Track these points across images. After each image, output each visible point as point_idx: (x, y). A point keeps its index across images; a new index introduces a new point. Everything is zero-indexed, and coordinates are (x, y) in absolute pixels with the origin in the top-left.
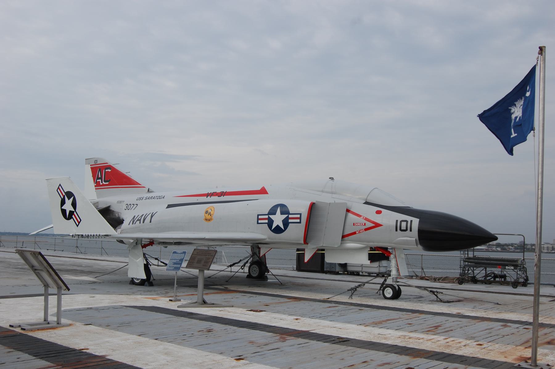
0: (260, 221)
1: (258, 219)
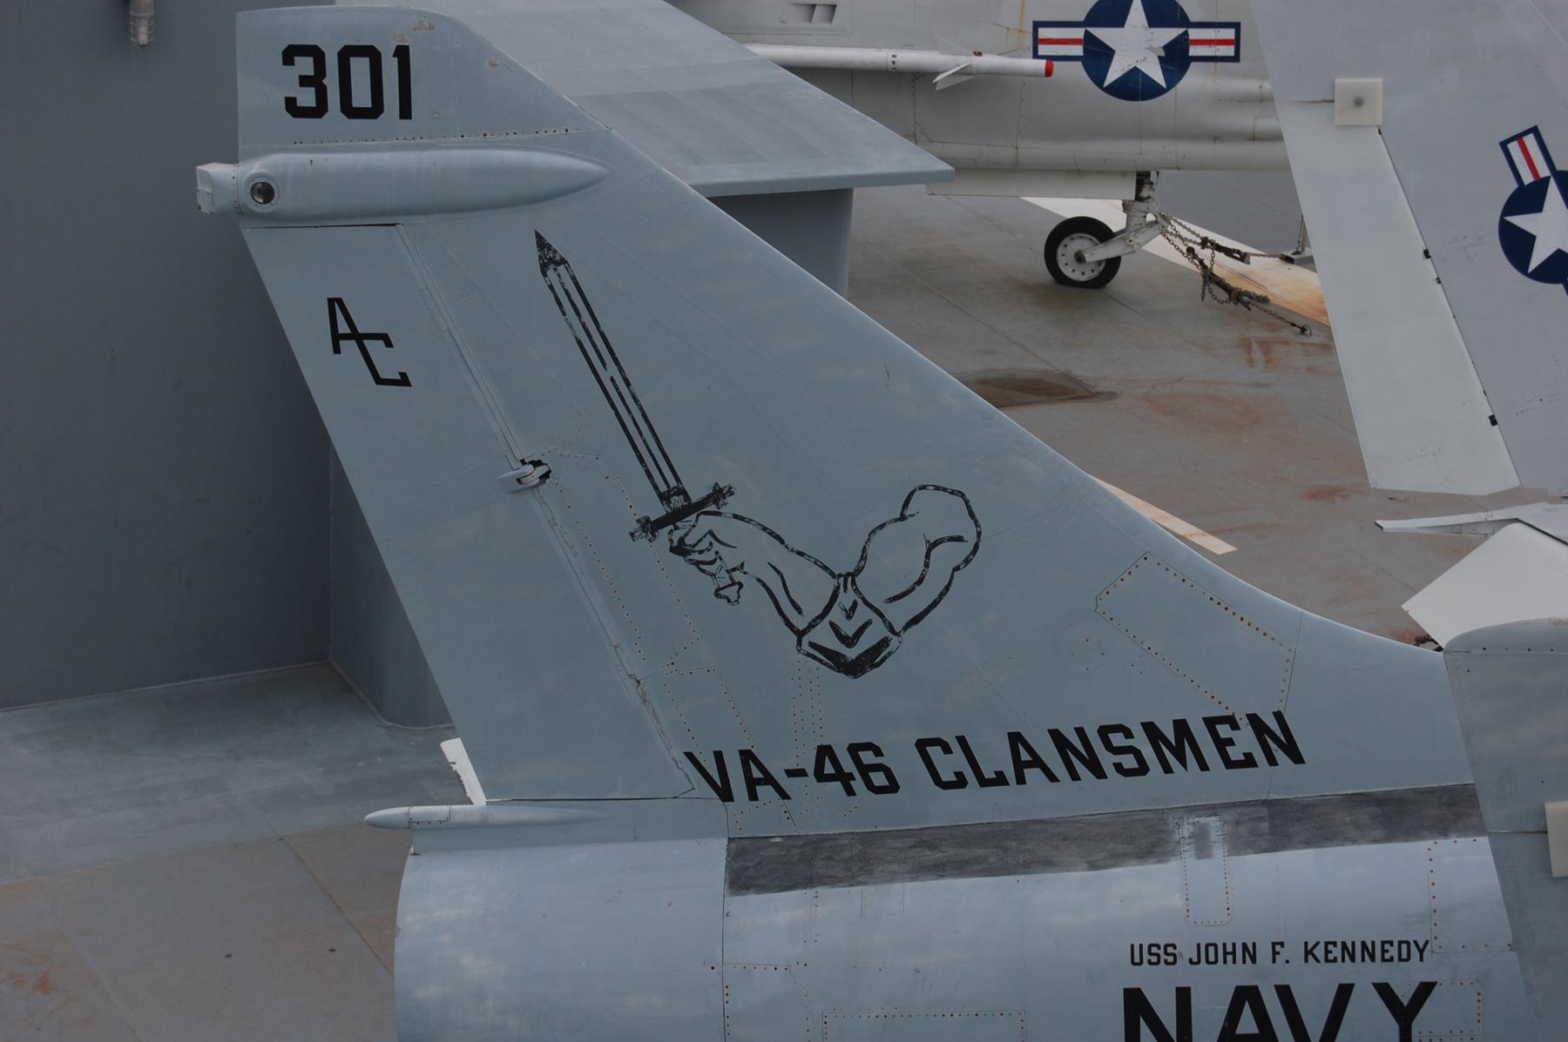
0: (1514, 147)
1: (1236, 42)
